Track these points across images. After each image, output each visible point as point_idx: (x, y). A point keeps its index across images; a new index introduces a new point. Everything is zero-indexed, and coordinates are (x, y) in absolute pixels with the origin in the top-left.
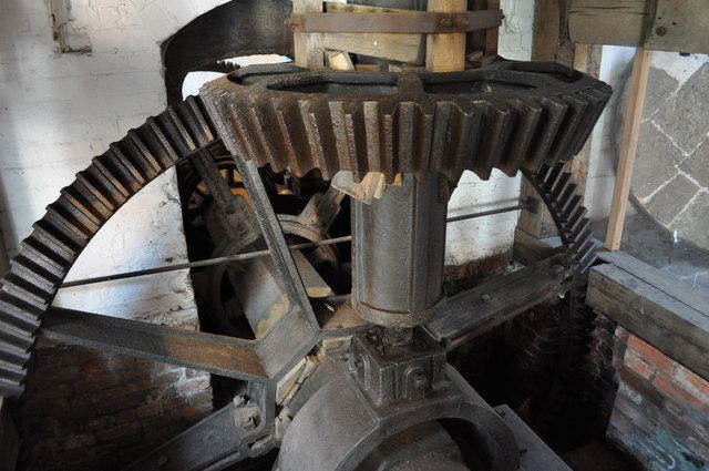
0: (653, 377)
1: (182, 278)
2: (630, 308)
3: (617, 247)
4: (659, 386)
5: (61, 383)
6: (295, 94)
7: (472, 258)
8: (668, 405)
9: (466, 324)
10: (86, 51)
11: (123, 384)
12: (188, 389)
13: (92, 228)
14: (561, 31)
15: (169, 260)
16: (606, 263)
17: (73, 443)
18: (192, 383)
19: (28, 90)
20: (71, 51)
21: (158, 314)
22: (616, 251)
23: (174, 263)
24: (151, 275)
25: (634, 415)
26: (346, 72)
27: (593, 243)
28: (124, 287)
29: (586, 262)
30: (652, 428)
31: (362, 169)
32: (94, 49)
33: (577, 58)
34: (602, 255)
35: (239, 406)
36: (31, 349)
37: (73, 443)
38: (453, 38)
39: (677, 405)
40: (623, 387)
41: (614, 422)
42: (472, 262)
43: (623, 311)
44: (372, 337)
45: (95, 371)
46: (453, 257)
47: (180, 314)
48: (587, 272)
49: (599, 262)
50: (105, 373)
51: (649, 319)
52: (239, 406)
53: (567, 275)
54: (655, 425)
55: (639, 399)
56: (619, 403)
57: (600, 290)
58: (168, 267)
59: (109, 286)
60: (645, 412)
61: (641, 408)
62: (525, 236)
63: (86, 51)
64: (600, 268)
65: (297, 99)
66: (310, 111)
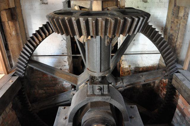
0: (184, 108)
1: (66, 58)
2: (181, 87)
3: (186, 69)
4: (185, 111)
5: (39, 78)
6: (87, 16)
7: (144, 66)
8: (186, 118)
9: (132, 82)
10: (47, 3)
11: (52, 81)
12: (66, 85)
13: (38, 43)
14: (175, 2)
15: (63, 54)
16: (180, 73)
17: (41, 91)
18: (67, 84)
19: (34, 12)
20: (44, 3)
21: (60, 66)
22: (186, 70)
23: (64, 55)
24: (58, 56)
25: (178, 119)
26: (77, 10)
27: (176, 66)
28: (53, 58)
29: (173, 72)
30: (182, 123)
31: (81, 34)
32: (48, 3)
33: (180, 11)
34: (179, 70)
35: (73, 91)
36: (25, 67)
37: (41, 91)
38: (98, 2)
39: (188, 118)
40: (177, 110)
41: (174, 120)
42: (144, 67)
43: (180, 87)
44: (92, 80)
45: (45, 76)
46: (139, 65)
47: (65, 67)
48: (173, 74)
49: (178, 72)
50: (48, 77)
51: (185, 91)
52: (73, 91)
53: (166, 74)
54: (183, 123)
55: (180, 114)
56: (175, 114)
57: (175, 80)
58: (63, 55)
59: (50, 58)
60: (181, 118)
61: (180, 117)
62: (161, 62)
63: (47, 3)
64: (177, 74)
65: (88, 18)
66: (74, 20)
